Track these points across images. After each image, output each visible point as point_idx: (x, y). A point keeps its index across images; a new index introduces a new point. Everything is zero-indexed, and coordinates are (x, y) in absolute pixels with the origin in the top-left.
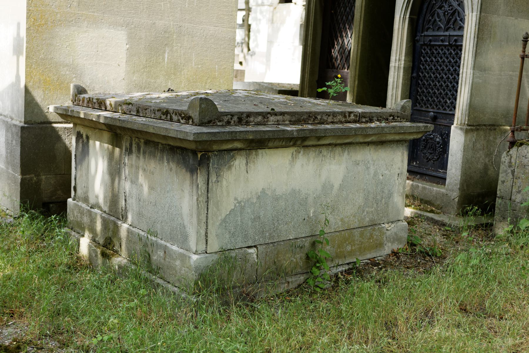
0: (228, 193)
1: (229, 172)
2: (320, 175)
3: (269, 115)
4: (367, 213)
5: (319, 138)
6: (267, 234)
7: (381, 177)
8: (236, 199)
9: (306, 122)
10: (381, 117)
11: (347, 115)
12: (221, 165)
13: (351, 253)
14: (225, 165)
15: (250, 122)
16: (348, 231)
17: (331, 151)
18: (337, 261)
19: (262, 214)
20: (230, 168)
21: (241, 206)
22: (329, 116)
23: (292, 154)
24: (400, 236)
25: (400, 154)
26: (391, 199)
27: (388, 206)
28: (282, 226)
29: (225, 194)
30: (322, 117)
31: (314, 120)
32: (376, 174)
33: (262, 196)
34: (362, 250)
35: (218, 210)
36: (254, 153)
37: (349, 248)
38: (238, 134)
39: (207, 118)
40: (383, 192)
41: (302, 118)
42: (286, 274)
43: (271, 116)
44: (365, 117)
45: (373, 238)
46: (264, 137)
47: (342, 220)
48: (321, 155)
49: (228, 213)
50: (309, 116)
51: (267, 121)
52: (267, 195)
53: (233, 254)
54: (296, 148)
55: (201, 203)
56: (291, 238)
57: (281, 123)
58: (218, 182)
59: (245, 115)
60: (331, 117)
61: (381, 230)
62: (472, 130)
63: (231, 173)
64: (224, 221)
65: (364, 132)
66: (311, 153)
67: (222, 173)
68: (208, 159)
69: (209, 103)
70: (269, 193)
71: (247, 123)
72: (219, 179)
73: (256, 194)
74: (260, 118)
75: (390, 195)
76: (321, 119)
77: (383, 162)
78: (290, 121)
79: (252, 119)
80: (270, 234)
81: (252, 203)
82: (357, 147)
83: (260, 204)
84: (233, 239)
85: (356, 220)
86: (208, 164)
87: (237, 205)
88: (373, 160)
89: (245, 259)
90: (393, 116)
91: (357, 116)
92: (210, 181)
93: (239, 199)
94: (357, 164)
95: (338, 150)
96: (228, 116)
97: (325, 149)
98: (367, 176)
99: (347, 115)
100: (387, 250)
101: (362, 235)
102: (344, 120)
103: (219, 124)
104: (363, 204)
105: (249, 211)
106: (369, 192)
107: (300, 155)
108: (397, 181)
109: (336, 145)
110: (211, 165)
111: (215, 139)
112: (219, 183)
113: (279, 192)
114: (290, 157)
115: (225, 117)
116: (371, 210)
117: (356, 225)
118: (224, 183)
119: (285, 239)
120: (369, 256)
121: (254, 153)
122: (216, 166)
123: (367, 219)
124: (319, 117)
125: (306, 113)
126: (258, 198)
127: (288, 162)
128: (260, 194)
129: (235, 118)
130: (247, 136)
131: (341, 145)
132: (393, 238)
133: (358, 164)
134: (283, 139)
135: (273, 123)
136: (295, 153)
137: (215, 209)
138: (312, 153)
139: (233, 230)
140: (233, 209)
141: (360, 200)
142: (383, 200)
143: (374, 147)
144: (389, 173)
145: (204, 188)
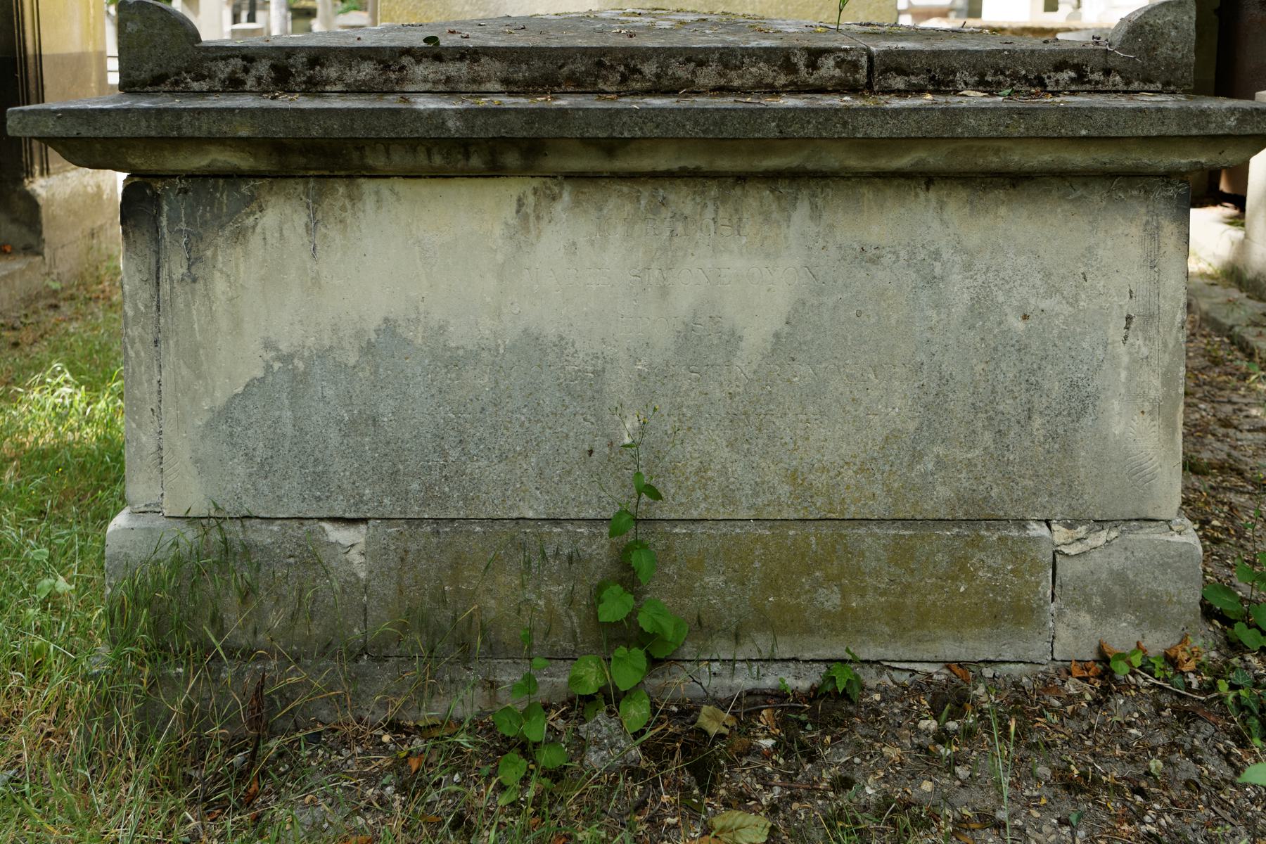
0: (237, 323)
1: (239, 249)
2: (664, 292)
3: (406, 60)
4: (939, 462)
5: (611, 147)
6: (415, 486)
7: (1020, 325)
8: (268, 345)
9: (548, 84)
10: (999, 71)
11: (800, 61)
12: (205, 223)
13: (839, 623)
14: (222, 227)
15: (327, 82)
16: (826, 530)
17: (722, 200)
18: (760, 644)
19: (386, 409)
20: (240, 235)
21: (291, 375)
22: (701, 64)
23: (520, 203)
24: (1153, 594)
25: (1135, 231)
26: (1087, 421)
27: (1067, 450)
28: (483, 463)
29: (224, 323)
30: (663, 66)
31: (624, 79)
32: (980, 307)
33: (384, 343)
34: (906, 618)
35: (199, 377)
36: (341, 190)
37: (830, 599)
38: (186, 117)
39: (147, 67)
40: (1033, 387)
41: (565, 70)
42: (493, 650)
43: (418, 62)
44: (901, 71)
45: (972, 577)
46: (302, 134)
47: (793, 477)
48: (666, 213)
49: (240, 390)
50: (600, 64)
51: (400, 81)
52: (409, 343)
53: (263, 536)
54: (536, 183)
55: (138, 345)
56: (531, 514)
57: (462, 87)
58: (194, 280)
59: (301, 59)
60: (713, 68)
61: (1020, 552)
62: (48, 169)
63: (246, 254)
64: (225, 414)
65: (945, 131)
66: (613, 203)
67: (209, 253)
68: (156, 200)
69: (155, 17)
70: (417, 336)
71: (313, 87)
72: (198, 270)
73: (359, 334)
74: (366, 70)
75: (1081, 402)
76: (658, 76)
77: (1022, 260)
78: (505, 81)
79: (333, 72)
80: (429, 488)
81: (341, 367)
82: (867, 193)
83: (376, 372)
84: (263, 485)
85: (878, 489)
86: (155, 220)
87: (277, 365)
88: (959, 248)
89: (312, 559)
90: (1078, 68)
91: (855, 66)
92: (164, 274)
93: (284, 347)
94: (869, 257)
95: (756, 200)
96: (232, 61)
97: (685, 190)
98: (931, 313)
99: (800, 61)
100: (1073, 636)
101: (901, 554)
102: (782, 80)
103: (196, 86)
104: (912, 426)
105: (330, 393)
106: (944, 380)
107: (558, 207)
108: (1122, 349)
109: (741, 178)
110: (164, 221)
111: (92, 134)
112: (199, 286)
113: (459, 336)
114: (509, 212)
115: (221, 64)
116: (960, 454)
117: (879, 509)
118: (220, 285)
119: (500, 514)
120: (951, 650)
121: (341, 190)
122: (183, 226)
123: (942, 491)
124: (649, 69)
125: (585, 51)
126: (368, 349)
127: (498, 230)
128: (373, 337)
129: (263, 69)
130: (225, 128)
131: (772, 178)
132: (1106, 594)
133: (875, 260)
134: (412, 144)
135: (428, 86)
136: (531, 199)
137: (185, 371)
138: (618, 206)
139: (261, 452)
140: (262, 380)
141: (895, 407)
142: (1037, 422)
143: (963, 194)
144: (1067, 310)
145: (146, 296)
